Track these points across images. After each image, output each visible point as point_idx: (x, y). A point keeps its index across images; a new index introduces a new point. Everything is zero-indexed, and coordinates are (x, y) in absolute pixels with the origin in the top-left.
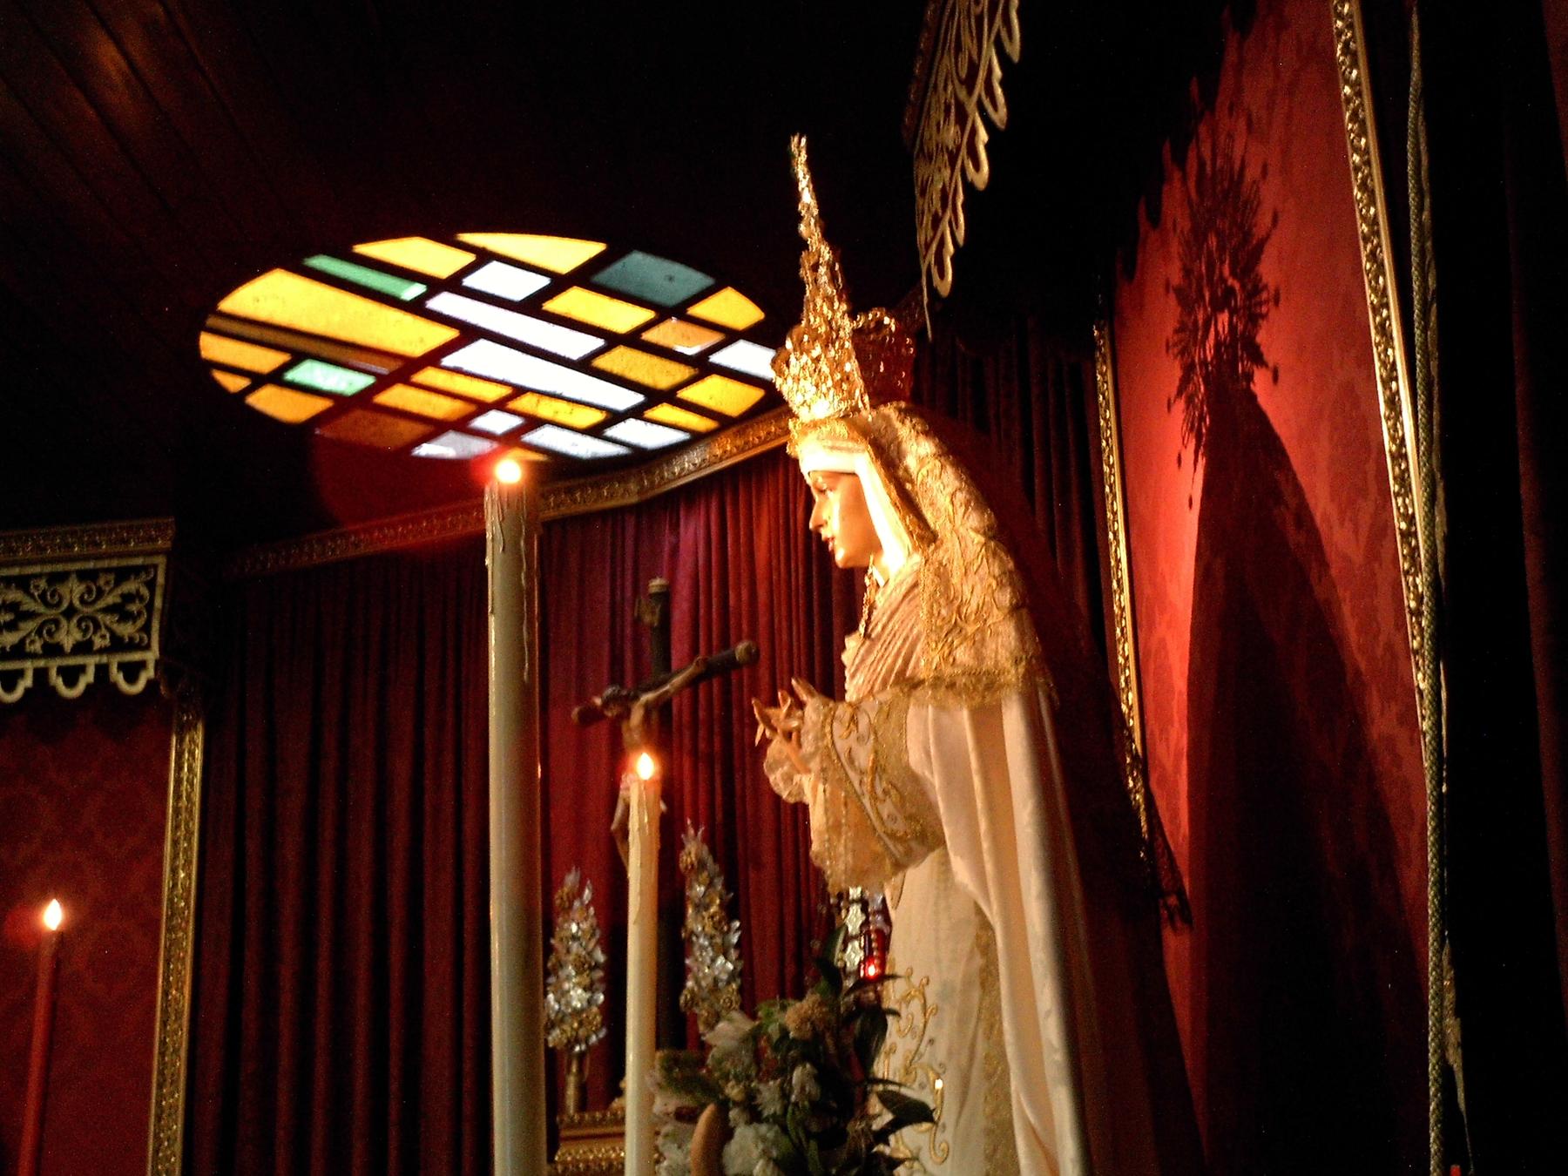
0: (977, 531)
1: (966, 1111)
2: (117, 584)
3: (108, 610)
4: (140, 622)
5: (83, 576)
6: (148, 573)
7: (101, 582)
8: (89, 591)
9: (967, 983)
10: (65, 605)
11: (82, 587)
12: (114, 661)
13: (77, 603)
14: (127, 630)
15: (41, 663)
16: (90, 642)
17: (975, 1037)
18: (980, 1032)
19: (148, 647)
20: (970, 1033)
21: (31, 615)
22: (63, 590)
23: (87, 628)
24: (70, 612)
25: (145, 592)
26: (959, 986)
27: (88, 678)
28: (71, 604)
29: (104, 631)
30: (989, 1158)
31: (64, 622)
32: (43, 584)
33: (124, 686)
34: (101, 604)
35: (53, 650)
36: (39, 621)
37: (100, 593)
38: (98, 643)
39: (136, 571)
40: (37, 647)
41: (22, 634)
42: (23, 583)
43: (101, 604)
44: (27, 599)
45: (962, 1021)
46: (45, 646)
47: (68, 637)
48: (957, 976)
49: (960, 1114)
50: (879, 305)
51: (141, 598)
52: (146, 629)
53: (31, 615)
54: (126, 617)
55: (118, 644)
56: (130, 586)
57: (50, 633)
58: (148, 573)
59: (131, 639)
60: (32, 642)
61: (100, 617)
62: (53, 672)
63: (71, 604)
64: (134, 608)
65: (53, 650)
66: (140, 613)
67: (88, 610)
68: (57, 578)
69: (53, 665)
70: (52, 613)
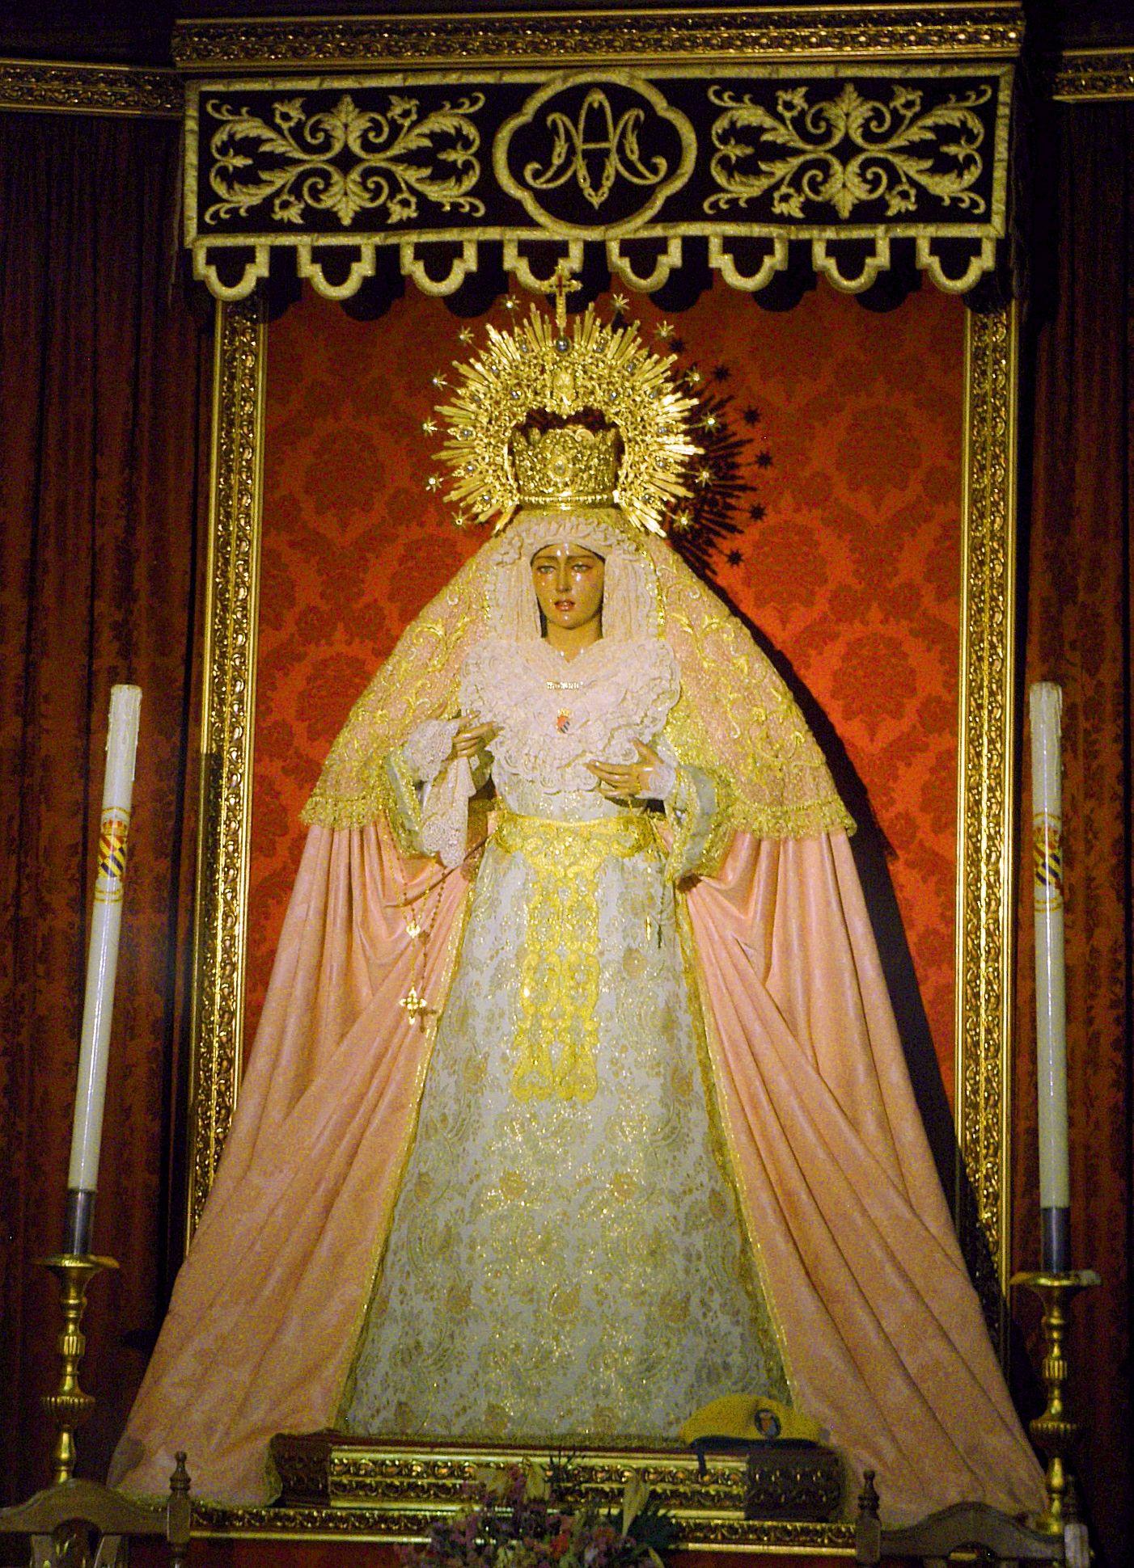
3: (914, 150)
4: (970, 177)
5: (870, 89)
7: (898, 103)
10: (337, 147)
11: (364, 123)
12: (924, 234)
14: (945, 187)
15: (492, 233)
16: (384, 212)
19: (985, 219)
21: (280, 162)
22: (835, 112)
23: (379, 187)
24: (346, 161)
25: (975, 125)
27: (363, 269)
28: (847, 138)
29: (406, 195)
32: (798, 98)
33: (733, 278)
34: (897, 142)
35: (820, 213)
36: (796, 162)
38: (896, 205)
39: (960, 88)
41: (765, 182)
42: (261, 106)
43: (897, 142)
46: (307, 212)
47: (346, 199)
51: (971, 138)
52: (983, 187)
53: (280, 162)
54: (945, 166)
55: (930, 209)
56: (949, 115)
57: (814, 186)
59: (456, 206)
61: (399, 170)
62: (614, 248)
63: (847, 138)
64: (735, 151)
65: (820, 213)
66: (970, 160)
67: (377, 160)
68: (324, 102)
69: (820, 238)
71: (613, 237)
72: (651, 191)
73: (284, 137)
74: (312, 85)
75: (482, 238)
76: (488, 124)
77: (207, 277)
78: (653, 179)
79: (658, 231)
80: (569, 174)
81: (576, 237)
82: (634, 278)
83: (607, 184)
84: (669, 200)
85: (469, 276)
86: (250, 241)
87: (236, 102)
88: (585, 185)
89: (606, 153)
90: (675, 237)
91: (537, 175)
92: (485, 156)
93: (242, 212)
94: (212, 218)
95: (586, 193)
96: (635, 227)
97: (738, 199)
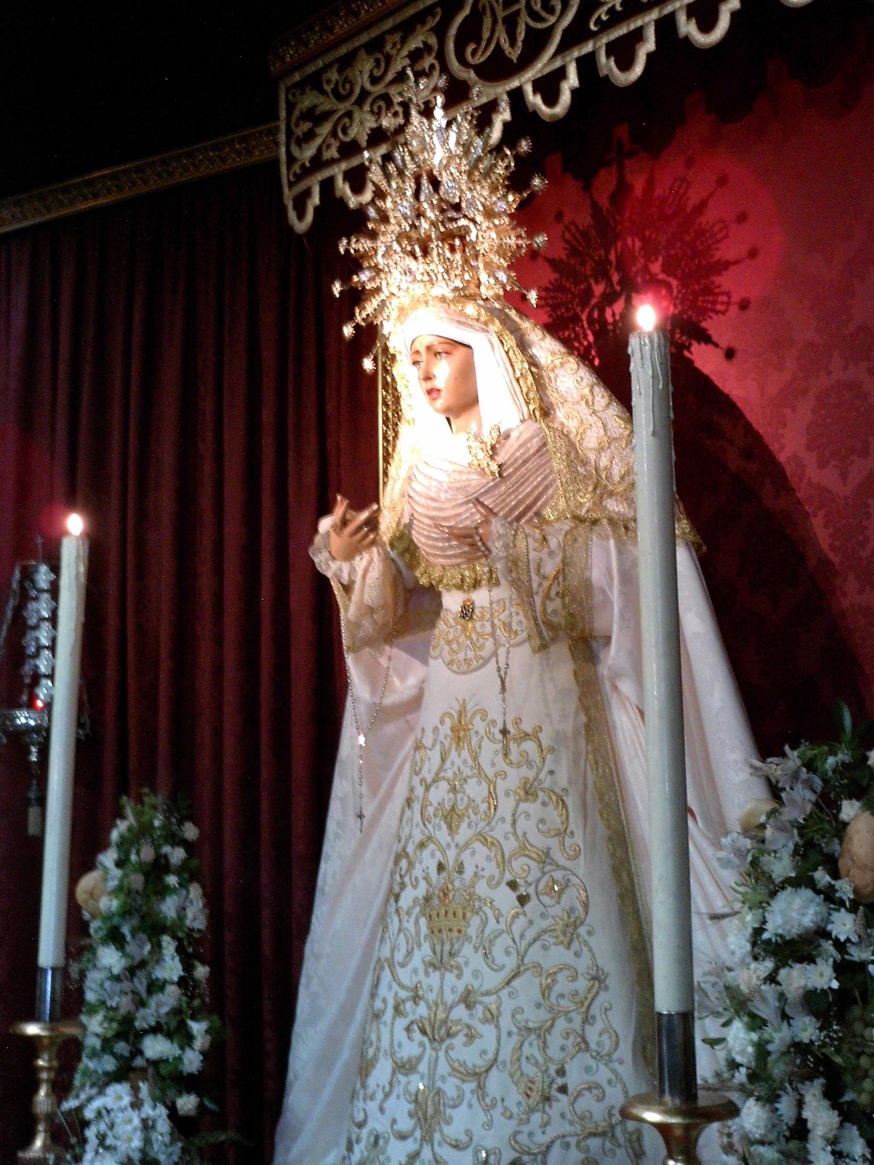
0: (542, 339)
1: (589, 826)
2: (404, 41)
6: (295, 174)
7: (388, 48)
8: (377, 61)
9: (576, 733)
10: (357, 90)
13: (368, 86)
17: (585, 772)
18: (588, 767)
20: (582, 770)
21: (326, 116)
26: (570, 735)
28: (363, 89)
30: (613, 855)
31: (356, 109)
32: (334, 76)
37: (389, 59)
40: (333, 153)
44: (322, 99)
45: (576, 761)
48: (568, 727)
49: (585, 833)
50: (338, 246)
53: (326, 116)
57: (345, 133)
58: (295, 174)
60: (329, 146)
62: (529, 89)
63: (363, 89)
67: (379, 89)
68: (347, 62)
70: (343, 107)
71: (525, 80)
72: (551, 29)
73: (328, 96)
74: (364, 38)
75: (508, 89)
76: (440, 31)
77: (689, 33)
78: (552, 19)
79: (558, 64)
80: (492, 46)
81: (501, 90)
82: (544, 108)
83: (521, 36)
84: (565, 32)
85: (574, 92)
86: (639, 23)
87: (301, 86)
88: (506, 46)
89: (518, 12)
90: (527, 82)
91: (474, 53)
92: (441, 57)
93: (308, 164)
94: (596, 24)
95: (507, 52)
96: (540, 67)
97: (613, 7)
